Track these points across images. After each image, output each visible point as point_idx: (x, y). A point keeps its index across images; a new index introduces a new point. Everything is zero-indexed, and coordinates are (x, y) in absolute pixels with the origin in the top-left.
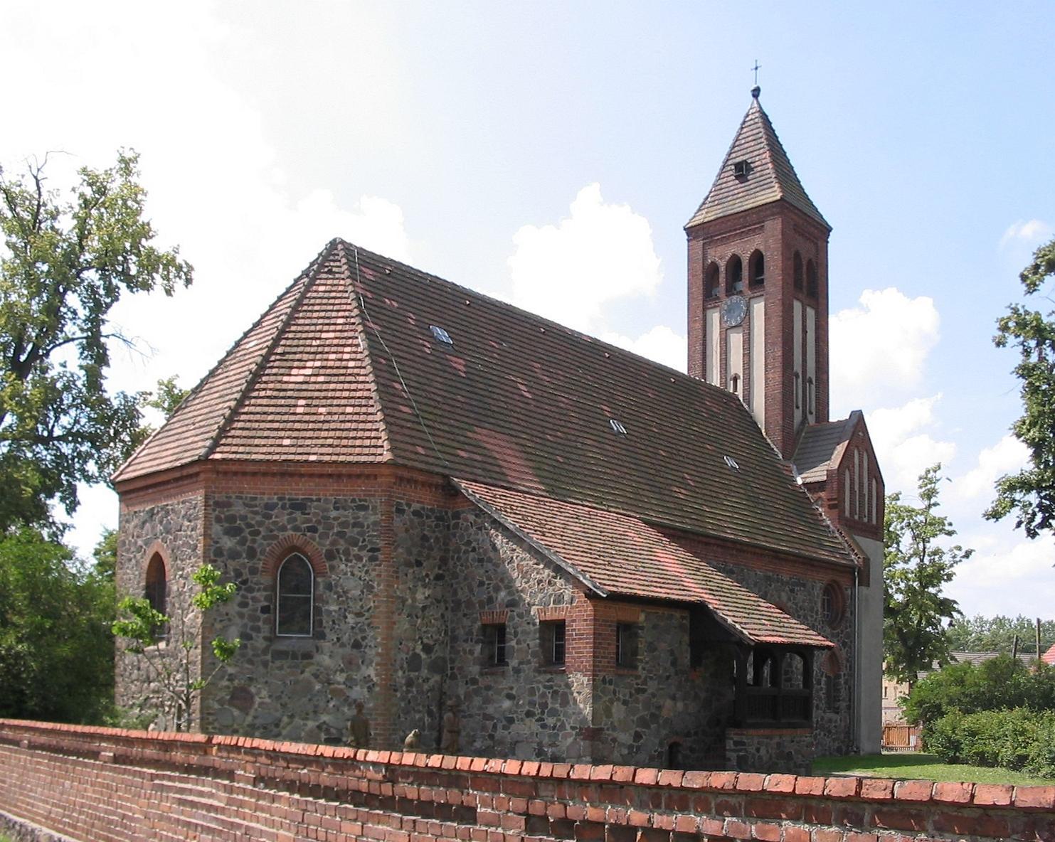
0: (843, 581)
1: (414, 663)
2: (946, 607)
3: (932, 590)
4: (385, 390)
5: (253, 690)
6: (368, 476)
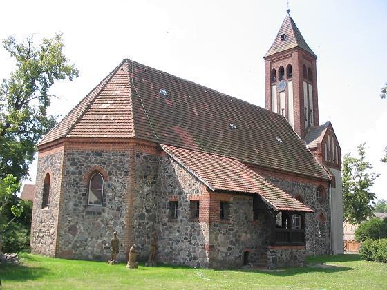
0: (325, 185)
1: (142, 216)
2: (371, 196)
3: (365, 189)
4: (136, 111)
5: (78, 227)
6: (126, 143)
